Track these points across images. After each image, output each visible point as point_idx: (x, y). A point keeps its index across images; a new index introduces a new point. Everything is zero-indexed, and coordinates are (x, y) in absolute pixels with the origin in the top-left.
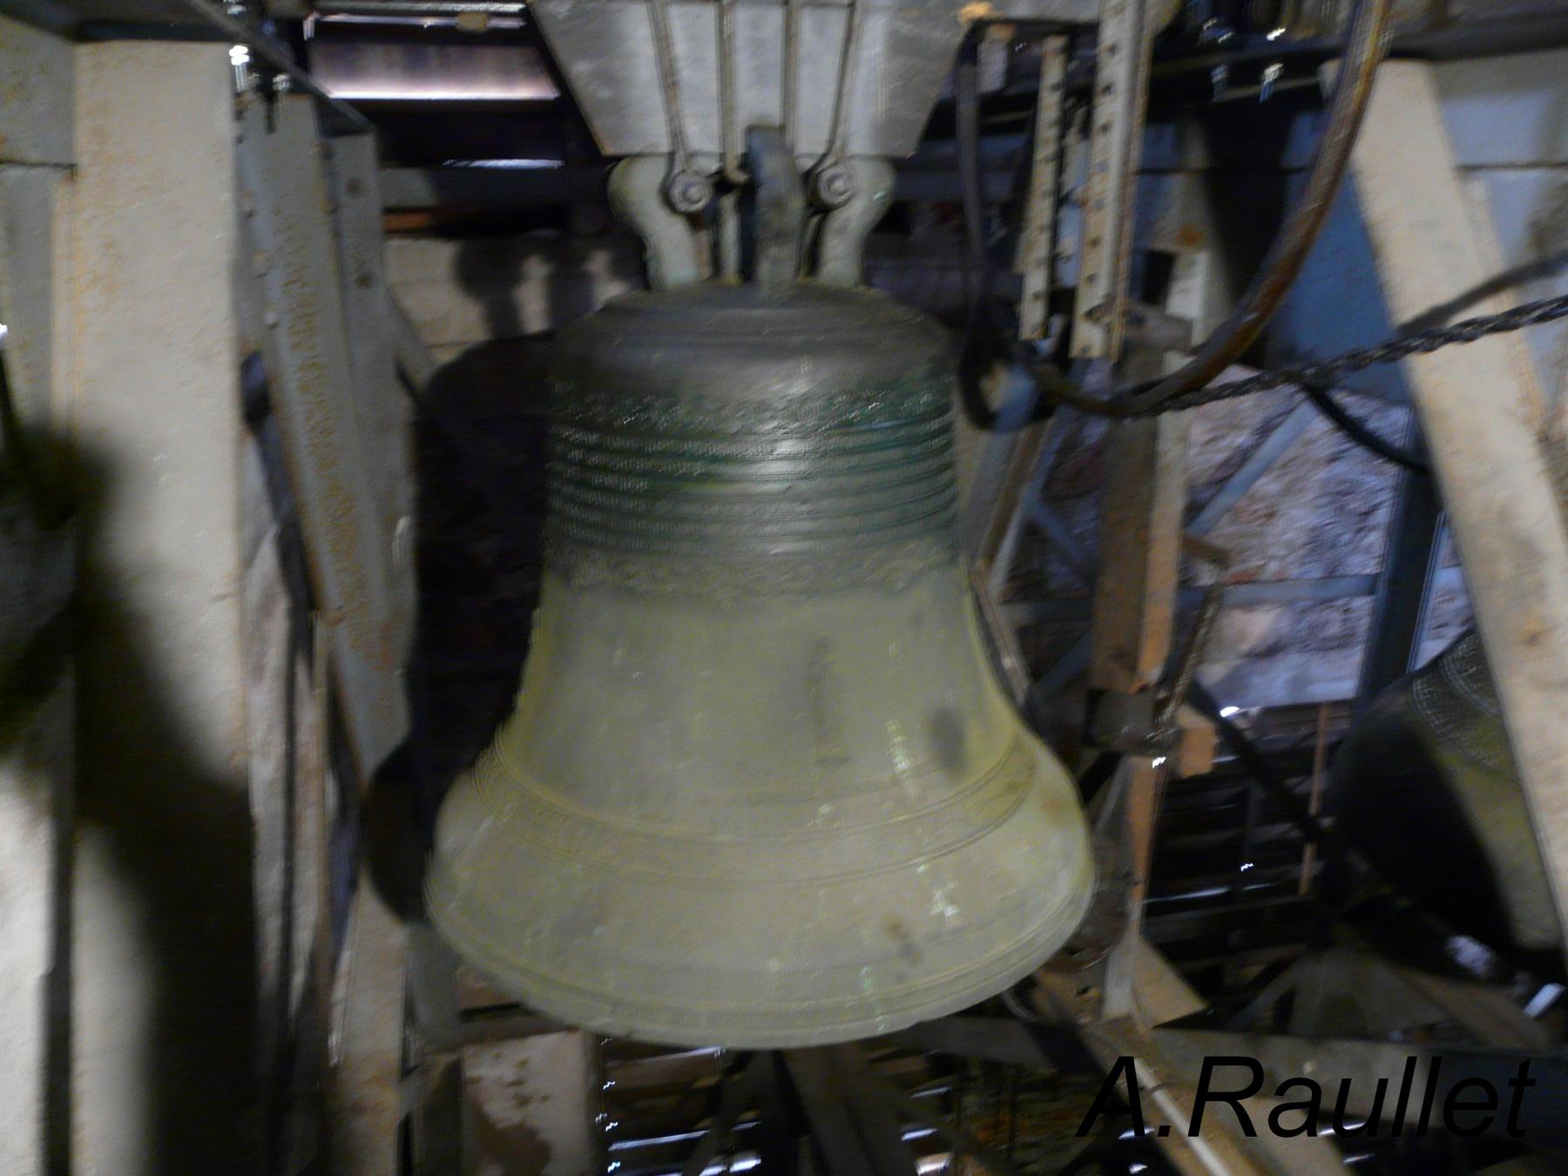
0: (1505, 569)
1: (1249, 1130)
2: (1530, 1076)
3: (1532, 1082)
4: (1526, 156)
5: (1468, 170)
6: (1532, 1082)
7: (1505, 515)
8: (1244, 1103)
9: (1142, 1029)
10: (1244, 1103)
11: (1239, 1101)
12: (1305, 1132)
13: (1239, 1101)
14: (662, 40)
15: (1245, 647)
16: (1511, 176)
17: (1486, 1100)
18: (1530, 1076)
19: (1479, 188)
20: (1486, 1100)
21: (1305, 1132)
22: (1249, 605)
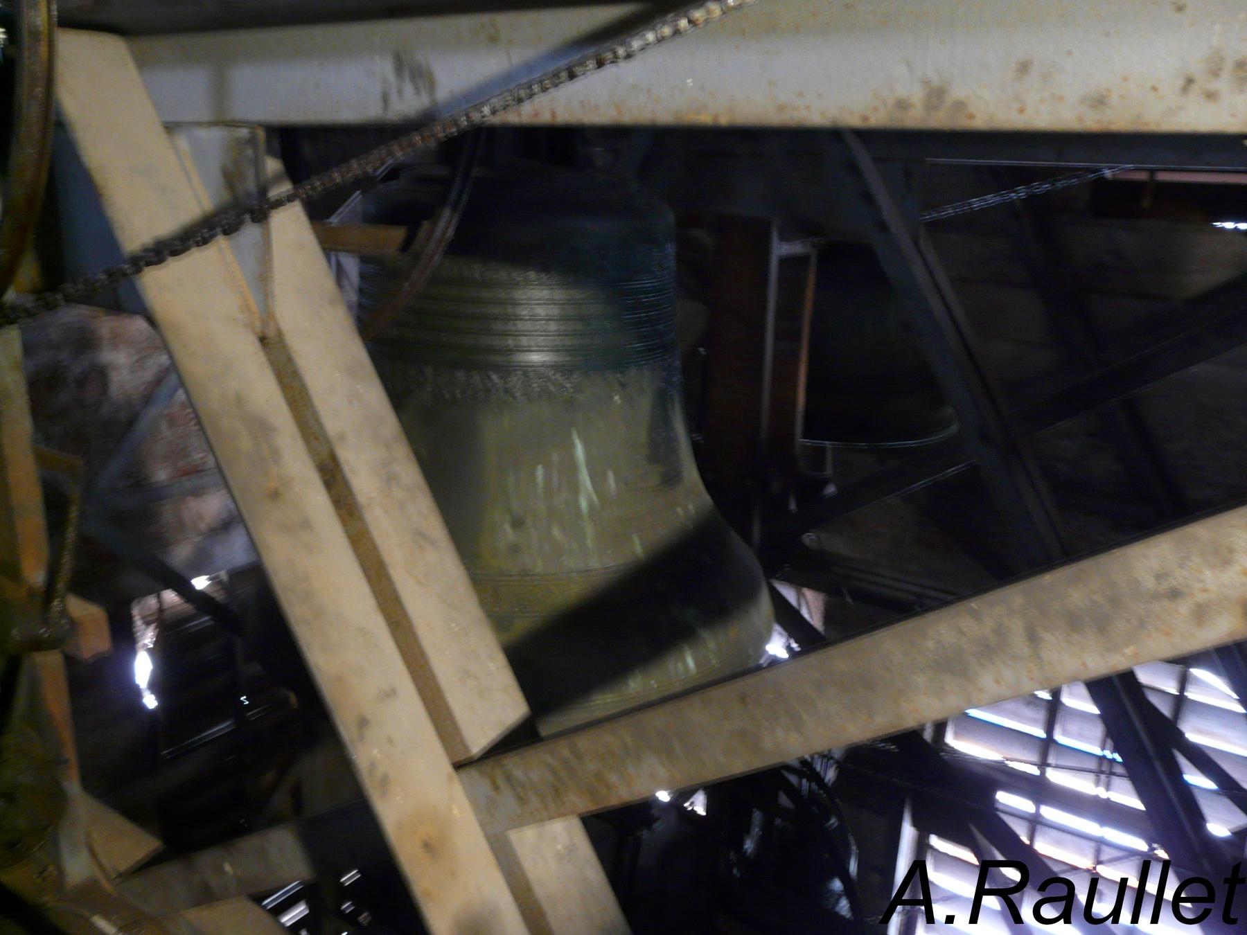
0: (245, 444)
1: (1017, 919)
2: (1240, 876)
3: (1242, 881)
4: (205, 116)
5: (171, 128)
6: (1242, 881)
7: (239, 401)
8: (1012, 896)
9: (107, 886)
10: (1012, 896)
11: (1010, 896)
12: (1062, 920)
13: (1010, 896)
14: (357, 197)
15: (203, 526)
16: (202, 133)
17: (1206, 895)
18: (1240, 876)
19: (183, 142)
20: (1206, 895)
21: (1062, 920)
22: (198, 493)
